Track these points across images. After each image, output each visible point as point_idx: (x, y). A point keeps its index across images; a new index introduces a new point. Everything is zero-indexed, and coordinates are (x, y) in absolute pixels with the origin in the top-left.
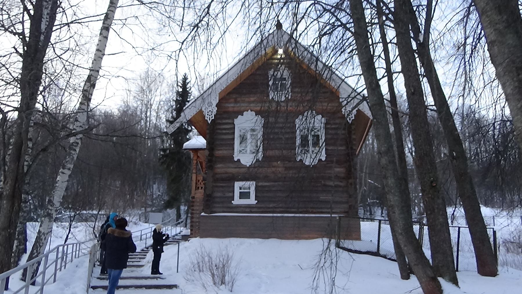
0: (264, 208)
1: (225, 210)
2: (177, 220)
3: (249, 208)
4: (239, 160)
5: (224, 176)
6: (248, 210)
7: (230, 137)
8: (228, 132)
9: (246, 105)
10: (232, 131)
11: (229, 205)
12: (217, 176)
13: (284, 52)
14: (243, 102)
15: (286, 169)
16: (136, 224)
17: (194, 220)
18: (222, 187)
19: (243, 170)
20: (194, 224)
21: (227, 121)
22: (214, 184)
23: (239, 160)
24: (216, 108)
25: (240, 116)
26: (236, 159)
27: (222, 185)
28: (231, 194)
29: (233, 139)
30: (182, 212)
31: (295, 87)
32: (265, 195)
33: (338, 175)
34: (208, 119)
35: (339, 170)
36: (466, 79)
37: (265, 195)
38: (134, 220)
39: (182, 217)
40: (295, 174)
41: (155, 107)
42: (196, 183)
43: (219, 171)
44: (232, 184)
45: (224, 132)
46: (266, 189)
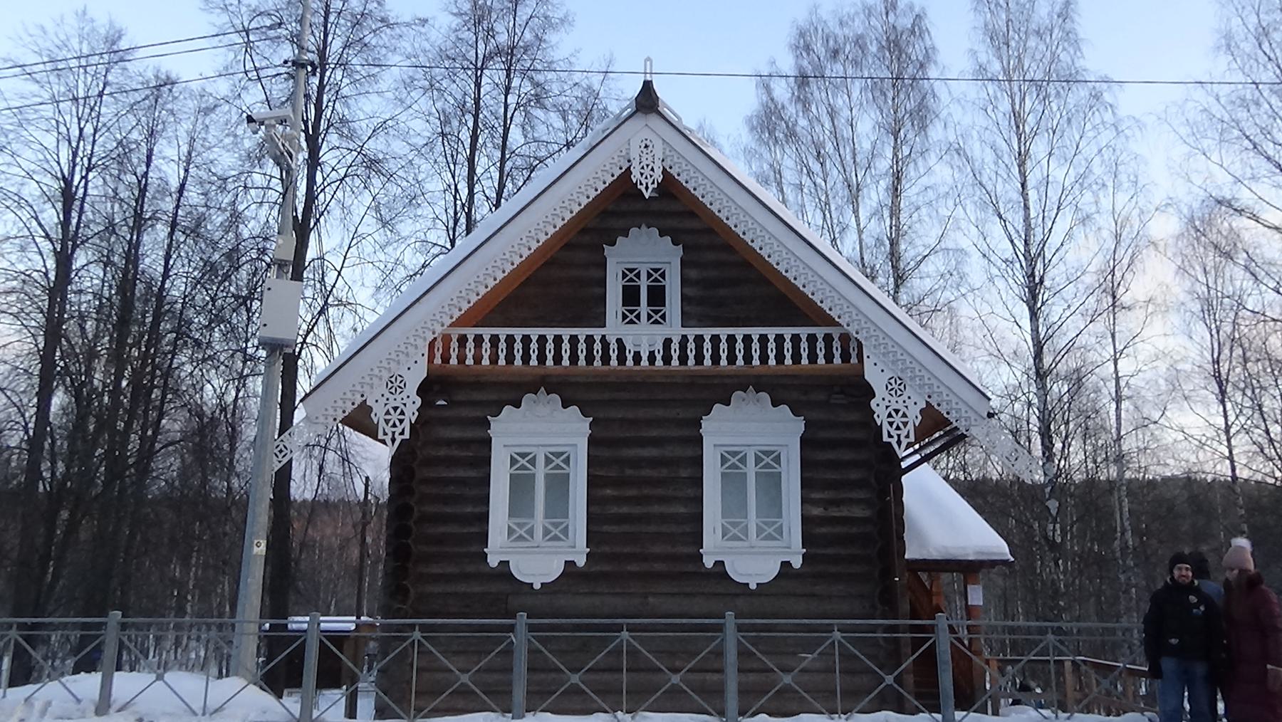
24: (419, 401)
29: (486, 481)
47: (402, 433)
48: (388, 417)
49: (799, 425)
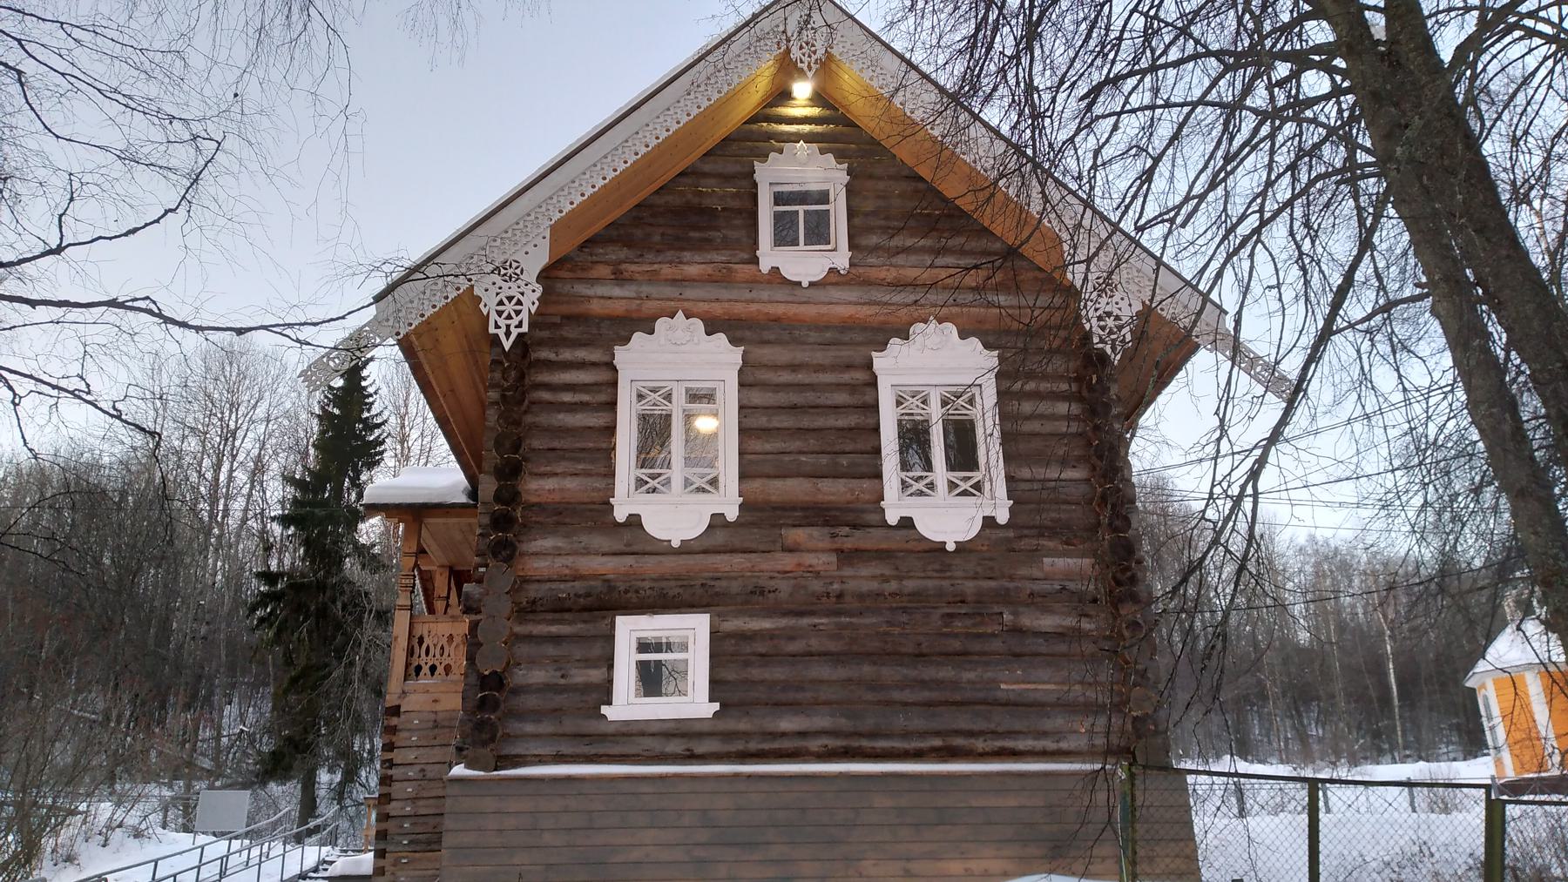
0: (746, 735)
1: (566, 749)
2: (303, 820)
3: (680, 739)
4: (634, 522)
5: (563, 590)
6: (675, 747)
7: (596, 420)
8: (585, 398)
9: (669, 291)
10: (602, 398)
11: (592, 726)
12: (533, 591)
13: (818, 98)
14: (653, 278)
15: (847, 557)
16: (138, 834)
17: (393, 808)
18: (556, 639)
19: (650, 565)
20: (390, 826)
21: (581, 354)
22: (518, 629)
23: (634, 522)
24: (539, 289)
25: (638, 337)
26: (620, 515)
27: (554, 629)
28: (595, 675)
29: (611, 430)
30: (322, 792)
31: (870, 230)
32: (756, 673)
33: (1071, 586)
34: (501, 333)
35: (1066, 565)
36: (1336, 305)
37: (756, 673)
38: (132, 819)
39: (321, 809)
40: (886, 580)
41: (247, 445)
42: (410, 652)
43: (539, 566)
44: (603, 626)
45: (567, 397)
46: (761, 648)
47: (520, 325)
48: (501, 308)
49: (735, 355)
